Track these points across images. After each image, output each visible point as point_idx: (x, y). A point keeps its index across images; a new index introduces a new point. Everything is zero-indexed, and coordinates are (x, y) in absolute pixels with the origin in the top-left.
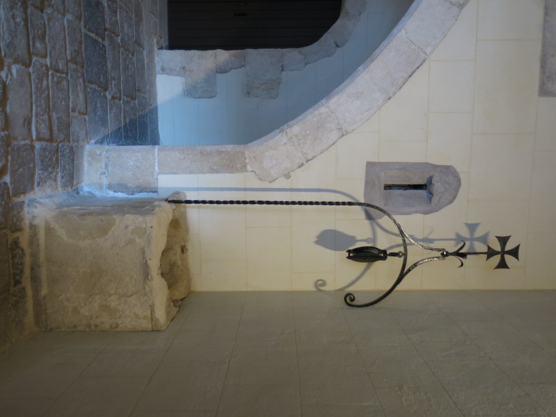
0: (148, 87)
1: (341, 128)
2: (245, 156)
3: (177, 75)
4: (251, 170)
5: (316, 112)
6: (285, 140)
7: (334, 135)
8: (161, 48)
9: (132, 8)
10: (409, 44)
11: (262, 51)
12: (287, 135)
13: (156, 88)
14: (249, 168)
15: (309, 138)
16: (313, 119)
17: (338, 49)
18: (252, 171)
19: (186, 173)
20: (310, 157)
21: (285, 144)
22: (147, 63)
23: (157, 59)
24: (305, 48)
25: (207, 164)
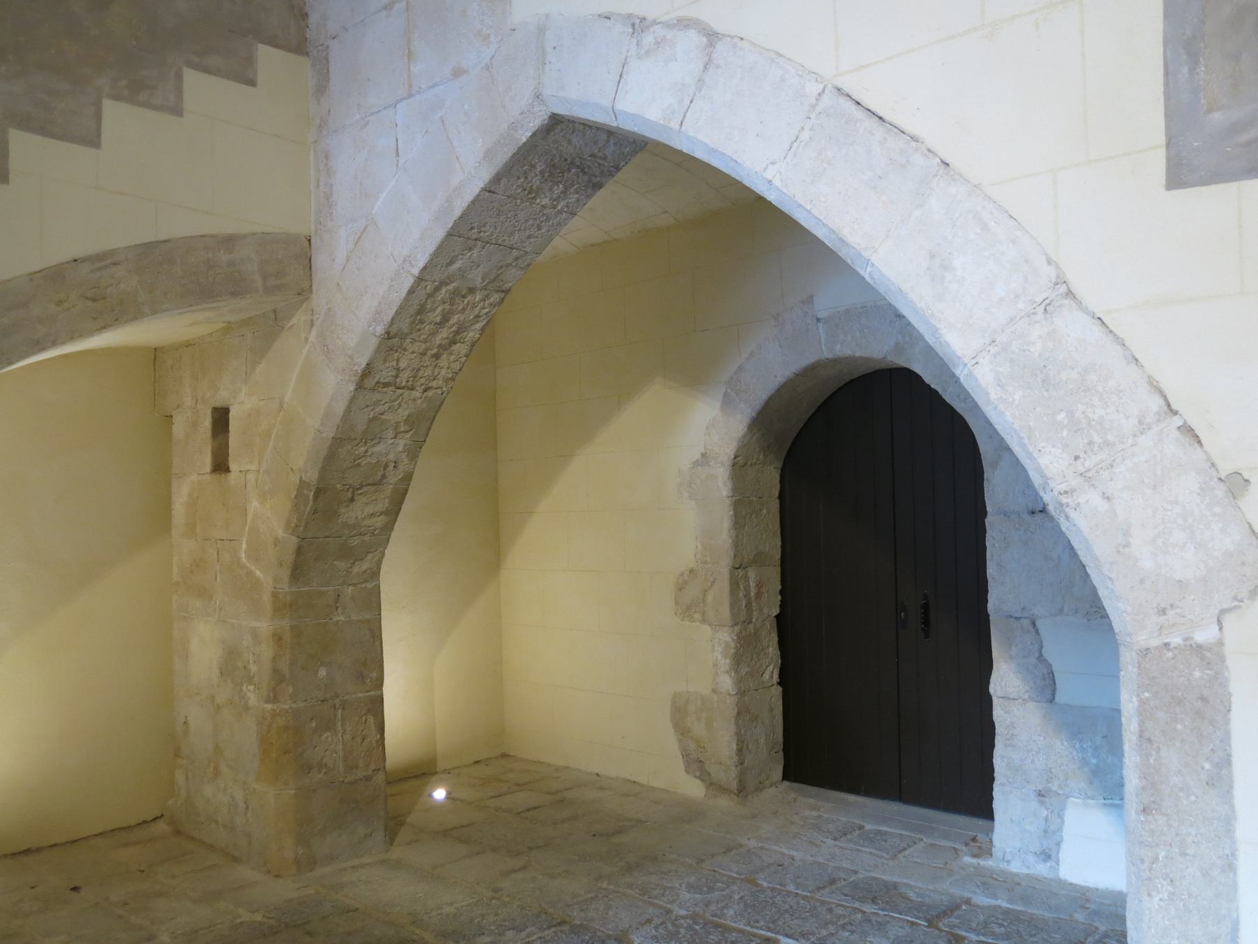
0: (1079, 916)
1: (1043, 305)
2: (1157, 648)
3: (1061, 817)
4: (1216, 628)
5: (994, 394)
6: (1090, 499)
7: (1071, 324)
8: (985, 850)
9: (848, 907)
10: (798, 148)
11: (991, 570)
12: (1073, 491)
13: (1097, 889)
14: (1204, 635)
15: (1083, 413)
16: (1017, 402)
19: (1234, 886)
20: (1155, 403)
22: (1010, 901)
23: (1015, 867)
24: (981, 450)
25: (1193, 798)
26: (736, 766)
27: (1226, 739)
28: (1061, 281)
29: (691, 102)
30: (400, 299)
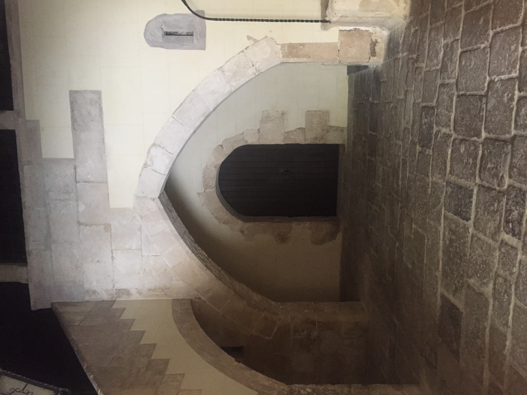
8: (343, 145)
11: (273, 143)
14: (280, 47)
17: (221, 143)
18: (278, 44)
21: (257, 62)
26: (312, 139)
27: (296, 44)
28: (219, 69)
29: (167, 151)
30: (215, 167)
